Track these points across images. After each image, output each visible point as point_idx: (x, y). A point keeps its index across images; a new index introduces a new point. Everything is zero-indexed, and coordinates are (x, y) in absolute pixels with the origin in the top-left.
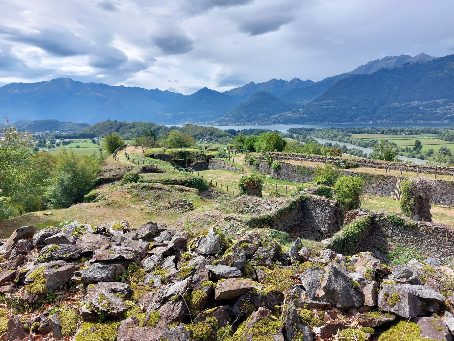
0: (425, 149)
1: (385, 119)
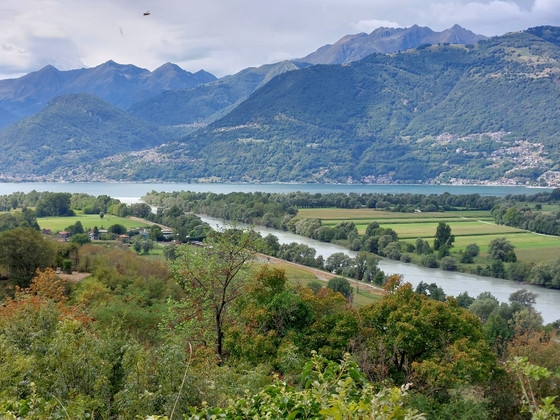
0: (460, 244)
1: (382, 174)
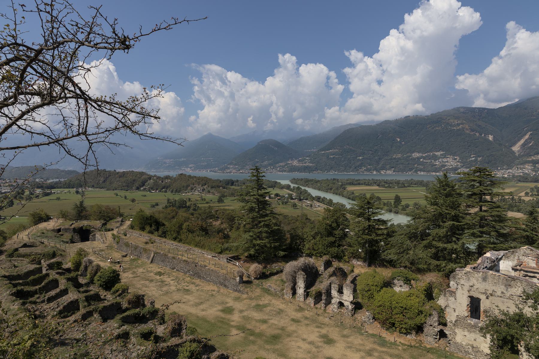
1: (389, 169)
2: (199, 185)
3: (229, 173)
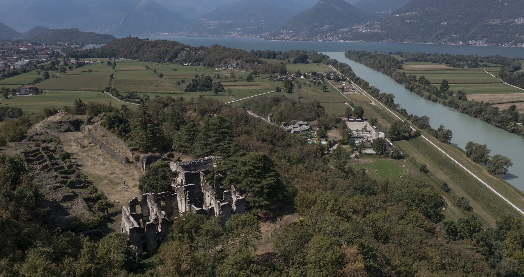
1: (480, 40)
2: (233, 59)
3: (281, 39)
